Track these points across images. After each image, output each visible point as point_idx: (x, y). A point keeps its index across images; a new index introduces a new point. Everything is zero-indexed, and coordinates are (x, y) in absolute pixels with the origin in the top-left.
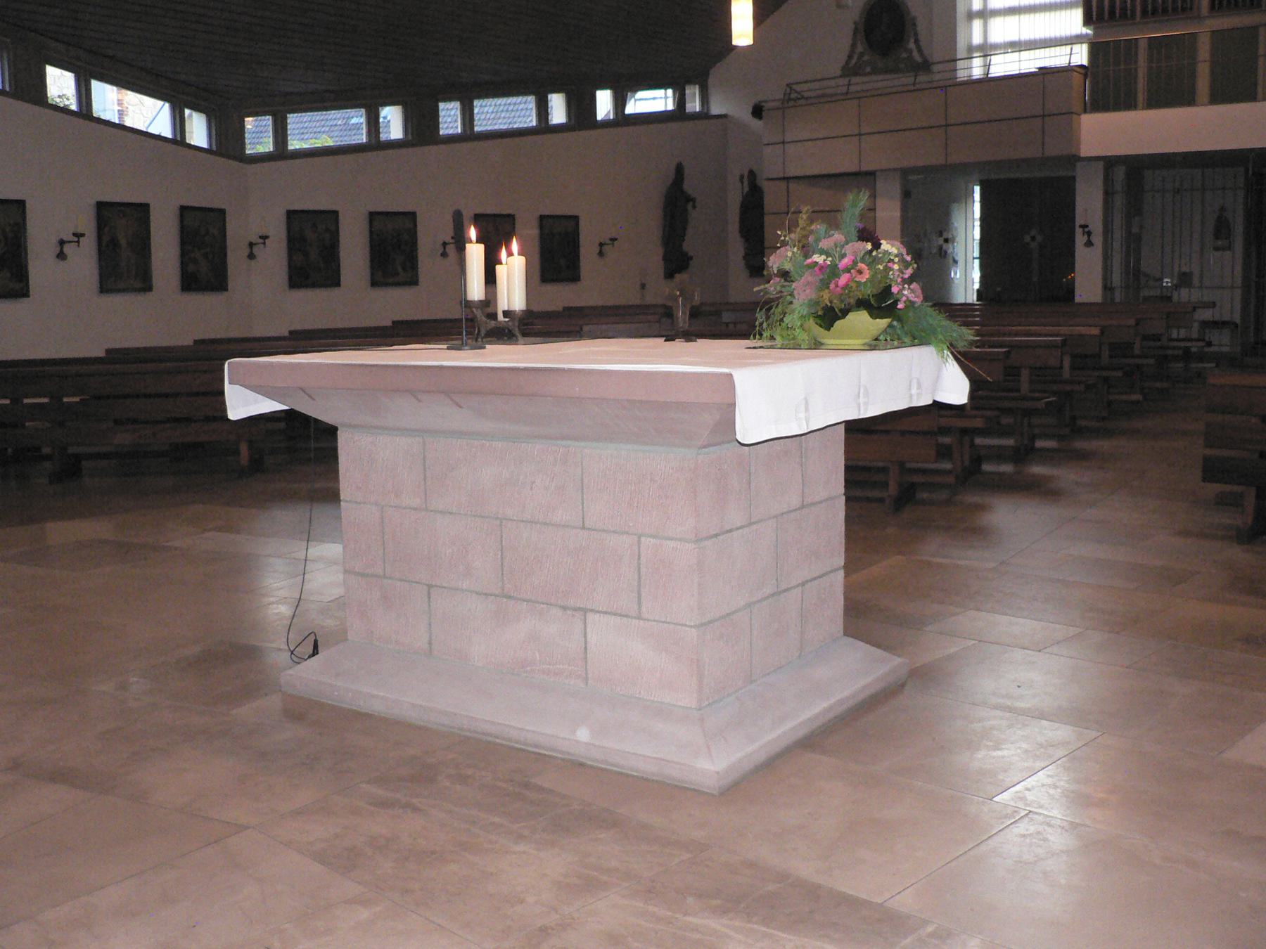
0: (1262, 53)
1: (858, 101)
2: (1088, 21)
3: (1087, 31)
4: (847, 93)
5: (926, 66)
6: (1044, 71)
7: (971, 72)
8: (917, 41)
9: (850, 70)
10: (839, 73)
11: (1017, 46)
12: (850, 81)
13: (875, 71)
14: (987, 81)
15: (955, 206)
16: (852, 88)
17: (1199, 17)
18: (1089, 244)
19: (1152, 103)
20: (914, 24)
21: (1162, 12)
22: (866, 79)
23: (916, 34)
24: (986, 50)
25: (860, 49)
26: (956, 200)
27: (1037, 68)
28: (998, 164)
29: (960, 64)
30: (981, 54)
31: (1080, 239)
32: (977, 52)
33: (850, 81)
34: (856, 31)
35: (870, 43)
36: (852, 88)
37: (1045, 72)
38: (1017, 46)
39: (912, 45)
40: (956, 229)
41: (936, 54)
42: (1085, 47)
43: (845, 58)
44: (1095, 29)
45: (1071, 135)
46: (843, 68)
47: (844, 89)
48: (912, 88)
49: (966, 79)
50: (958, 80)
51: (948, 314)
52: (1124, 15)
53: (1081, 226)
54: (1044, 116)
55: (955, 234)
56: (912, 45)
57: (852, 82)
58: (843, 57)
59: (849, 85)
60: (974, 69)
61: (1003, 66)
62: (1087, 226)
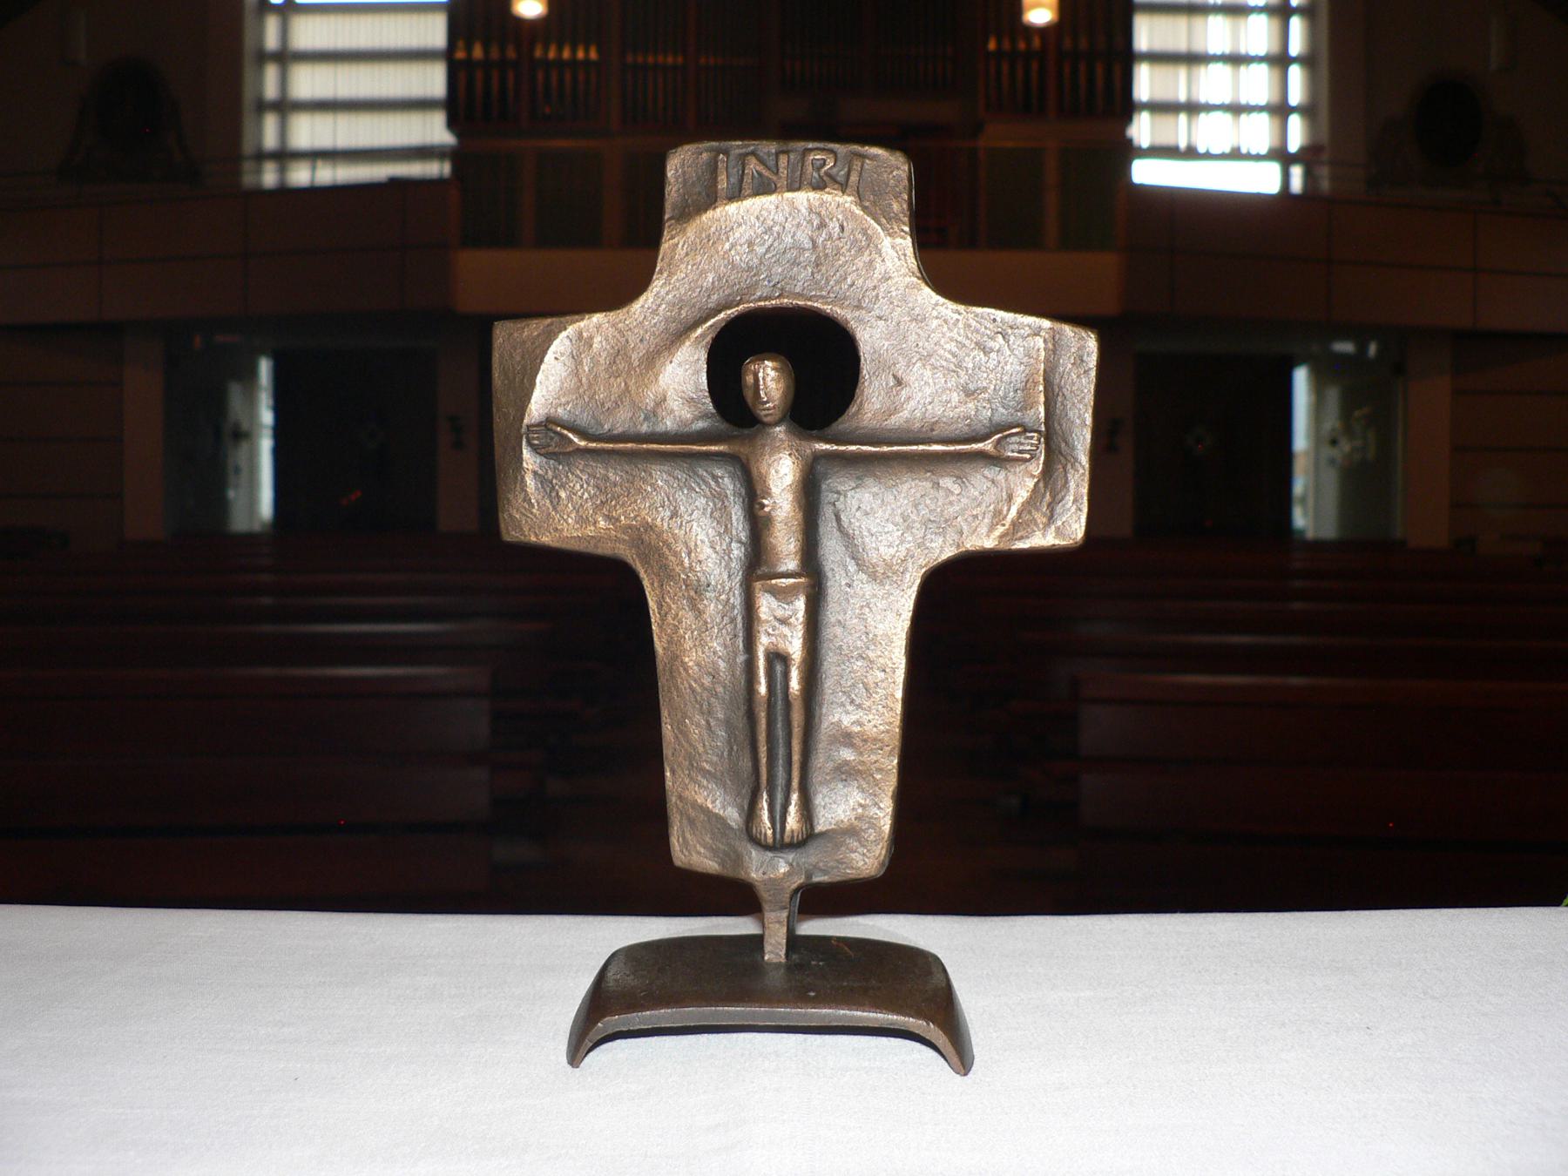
2: (452, 124)
14: (287, 195)
24: (285, 156)
29: (248, 166)
61: (301, 176)
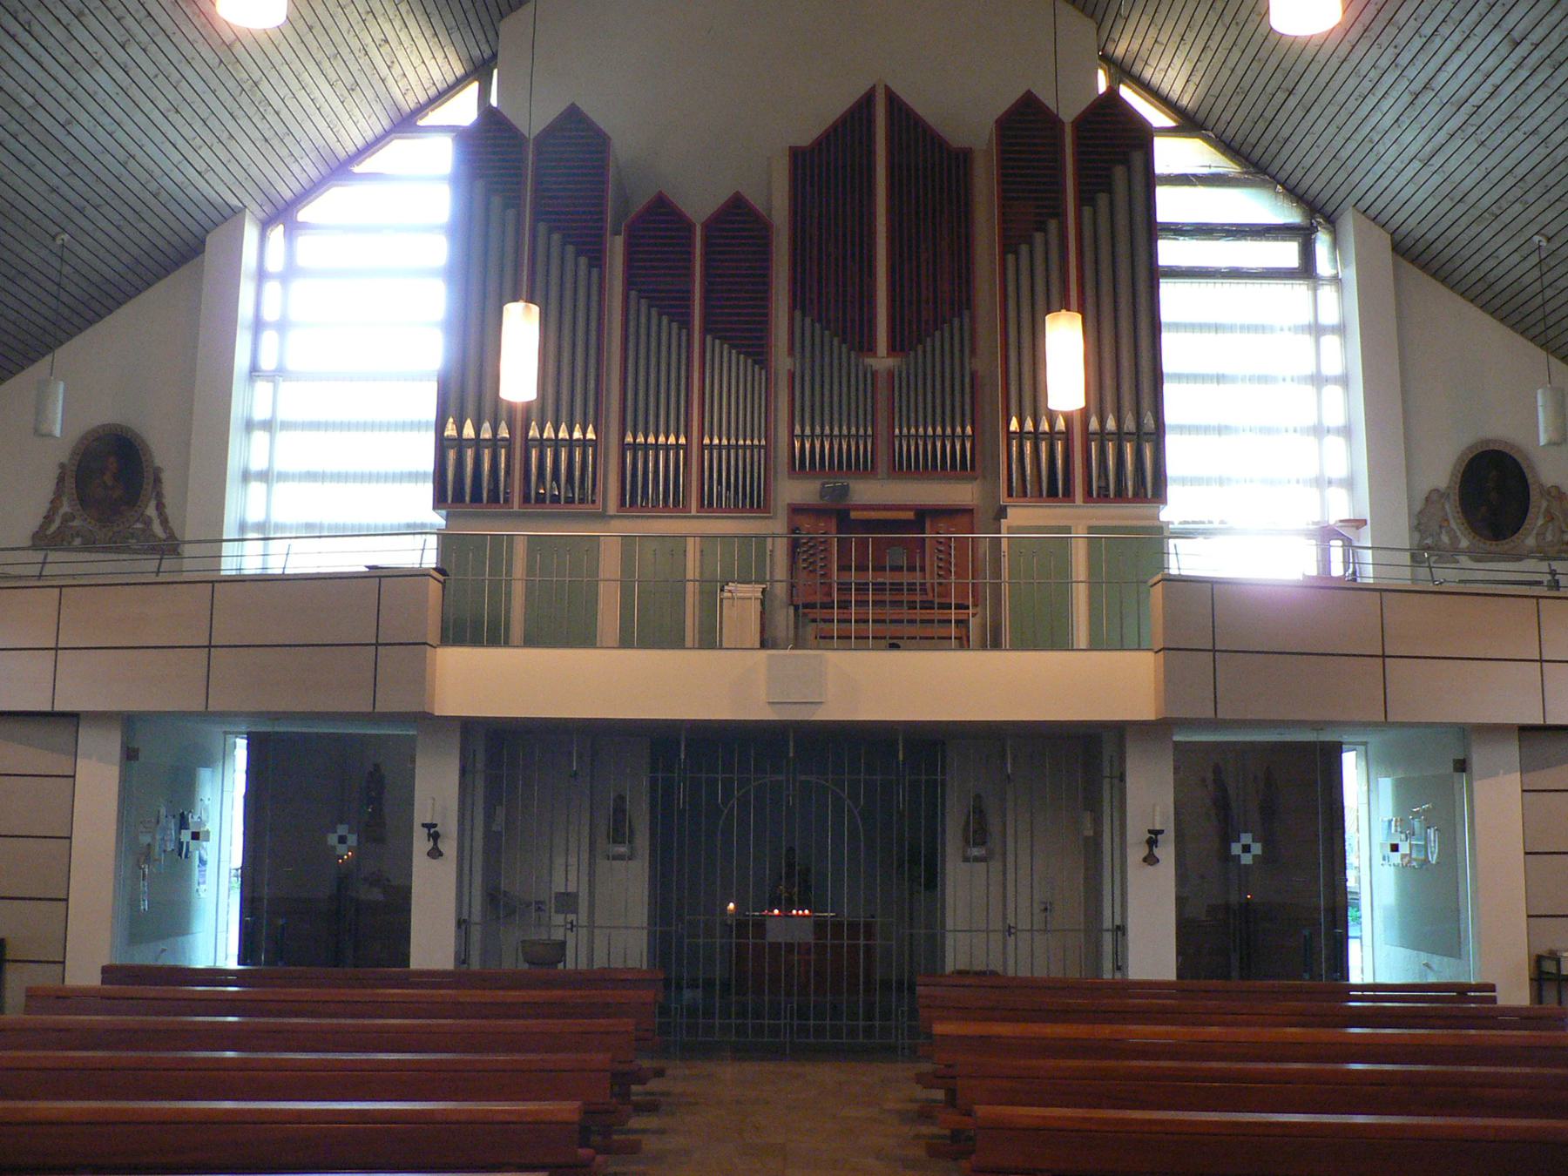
0: (519, 576)
1: (59, 589)
3: (438, 520)
4: (40, 576)
5: (170, 547)
6: (378, 573)
7: (219, 563)
8: (160, 506)
9: (44, 540)
10: (28, 543)
11: (314, 532)
12: (45, 557)
13: (90, 545)
15: (205, 774)
16: (48, 570)
17: (603, 516)
18: (435, 853)
19: (530, 641)
20: (158, 480)
21: (471, 501)
22: (74, 556)
23: (159, 496)
25: (65, 508)
26: (208, 762)
27: (367, 567)
28: (276, 716)
29: (227, 548)
30: (261, 536)
31: (421, 844)
32: (253, 531)
33: (45, 557)
34: (61, 480)
35: (83, 500)
36: (48, 570)
37: (377, 575)
38: (314, 532)
39: (151, 511)
40: (206, 809)
41: (190, 530)
42: (432, 541)
43: (39, 521)
44: (447, 518)
45: (420, 679)
46: (35, 536)
47: (35, 570)
48: (153, 578)
49: (234, 573)
50: (223, 573)
51: (1502, 772)
52: (494, 498)
53: (424, 825)
54: (56, 649)
55: (204, 818)
56: (151, 511)
57: (49, 560)
58: (34, 523)
59: (44, 563)
60: (223, 559)
62: (435, 826)
